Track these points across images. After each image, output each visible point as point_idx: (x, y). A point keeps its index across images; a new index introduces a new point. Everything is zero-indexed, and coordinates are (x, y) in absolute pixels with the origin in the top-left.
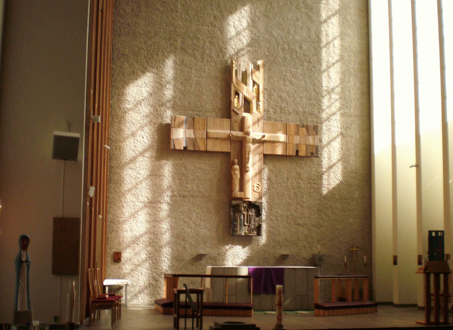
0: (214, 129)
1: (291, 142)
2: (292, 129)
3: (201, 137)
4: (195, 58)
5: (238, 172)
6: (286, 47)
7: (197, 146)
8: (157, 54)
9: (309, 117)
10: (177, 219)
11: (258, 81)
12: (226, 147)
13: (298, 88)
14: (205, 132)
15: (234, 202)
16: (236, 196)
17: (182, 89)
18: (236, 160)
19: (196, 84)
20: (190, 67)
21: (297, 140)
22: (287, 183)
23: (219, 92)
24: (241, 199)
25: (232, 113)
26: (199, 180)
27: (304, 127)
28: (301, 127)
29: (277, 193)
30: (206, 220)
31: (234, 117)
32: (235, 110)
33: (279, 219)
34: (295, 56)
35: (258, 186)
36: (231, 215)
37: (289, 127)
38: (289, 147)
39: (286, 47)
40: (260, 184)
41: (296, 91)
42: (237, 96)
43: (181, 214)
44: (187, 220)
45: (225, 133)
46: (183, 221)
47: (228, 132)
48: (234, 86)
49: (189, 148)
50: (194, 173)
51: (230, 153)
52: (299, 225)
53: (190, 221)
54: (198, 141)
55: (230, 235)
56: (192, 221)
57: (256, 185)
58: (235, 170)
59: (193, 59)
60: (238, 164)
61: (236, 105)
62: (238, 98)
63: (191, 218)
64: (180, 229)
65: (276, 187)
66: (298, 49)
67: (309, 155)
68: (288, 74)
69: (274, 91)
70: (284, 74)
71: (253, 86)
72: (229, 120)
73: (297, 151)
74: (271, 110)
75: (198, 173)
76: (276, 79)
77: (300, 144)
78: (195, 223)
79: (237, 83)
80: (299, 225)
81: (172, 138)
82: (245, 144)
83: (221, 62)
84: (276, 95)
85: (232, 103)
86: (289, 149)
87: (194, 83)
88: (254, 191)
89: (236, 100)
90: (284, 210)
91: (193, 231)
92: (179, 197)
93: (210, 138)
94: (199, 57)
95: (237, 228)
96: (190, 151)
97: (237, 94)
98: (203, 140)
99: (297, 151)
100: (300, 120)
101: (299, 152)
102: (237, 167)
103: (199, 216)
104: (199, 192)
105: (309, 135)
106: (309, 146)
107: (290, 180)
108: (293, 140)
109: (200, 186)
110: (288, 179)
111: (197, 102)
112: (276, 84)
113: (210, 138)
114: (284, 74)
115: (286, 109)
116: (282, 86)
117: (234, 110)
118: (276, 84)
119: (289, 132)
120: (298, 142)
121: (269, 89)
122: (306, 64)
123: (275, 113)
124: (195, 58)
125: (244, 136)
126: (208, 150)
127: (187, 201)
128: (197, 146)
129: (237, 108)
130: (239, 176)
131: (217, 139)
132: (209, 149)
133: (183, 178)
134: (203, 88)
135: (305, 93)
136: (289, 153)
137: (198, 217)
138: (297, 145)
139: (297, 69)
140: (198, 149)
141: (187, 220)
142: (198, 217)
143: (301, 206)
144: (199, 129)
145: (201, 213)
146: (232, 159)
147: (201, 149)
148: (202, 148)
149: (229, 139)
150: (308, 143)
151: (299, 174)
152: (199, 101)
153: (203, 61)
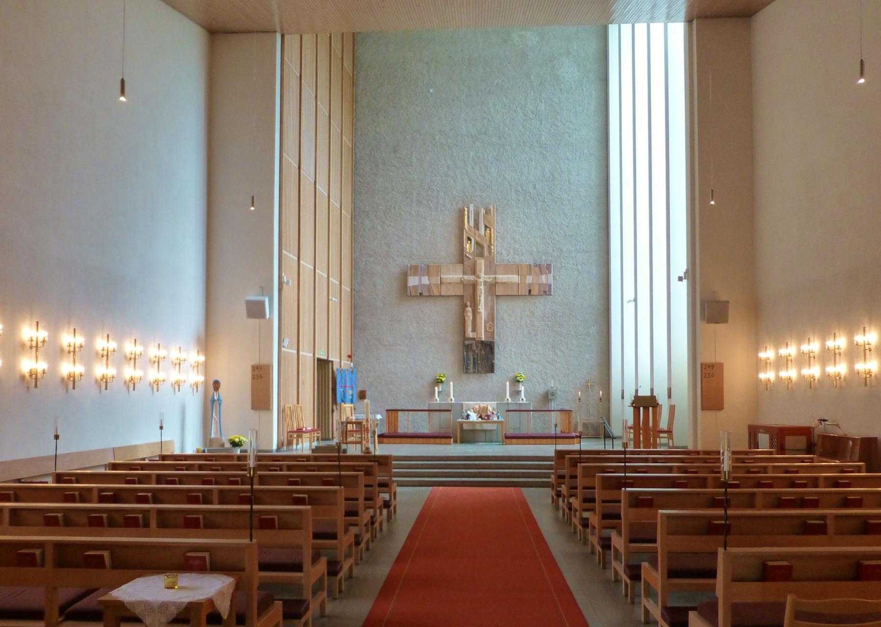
4: (430, 208)
5: (470, 314)
6: (520, 189)
8: (394, 208)
12: (459, 291)
15: (467, 342)
18: (469, 304)
21: (529, 279)
23: (453, 238)
24: (473, 339)
31: (466, 263)
34: (528, 197)
39: (520, 189)
49: (424, 294)
52: (532, 361)
57: (488, 325)
66: (531, 190)
68: (522, 216)
73: (530, 291)
74: (504, 252)
80: (532, 361)
89: (468, 245)
97: (469, 239)
99: (530, 291)
102: (469, 309)
122: (540, 204)
124: (430, 208)
130: (471, 318)
138: (530, 284)
148: (436, 293)
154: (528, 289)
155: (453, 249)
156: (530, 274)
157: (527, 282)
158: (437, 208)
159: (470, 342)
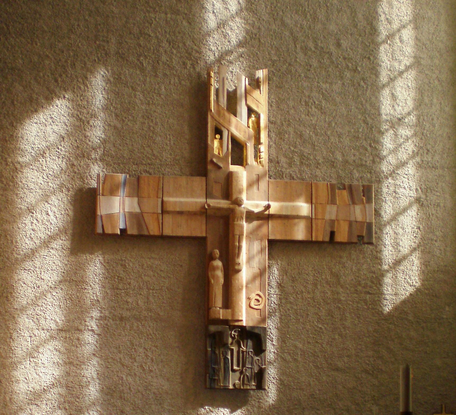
0: (177, 196)
1: (320, 217)
2: (323, 193)
3: (151, 211)
4: (142, 70)
5: (220, 274)
7: (145, 228)
9: (355, 171)
10: (110, 360)
11: (258, 107)
12: (197, 229)
13: (334, 118)
14: (160, 200)
15: (213, 328)
16: (217, 316)
17: (119, 126)
19: (143, 117)
20: (132, 88)
21: (331, 212)
22: (314, 293)
23: (186, 129)
24: (225, 322)
25: (210, 167)
26: (149, 289)
27: (344, 189)
28: (339, 189)
29: (296, 310)
30: (162, 361)
31: (213, 175)
32: (215, 160)
33: (299, 359)
35: (258, 298)
36: (207, 351)
37: (317, 190)
38: (317, 225)
40: (261, 294)
41: (330, 123)
42: (218, 136)
43: (115, 351)
44: (127, 361)
45: (196, 202)
46: (121, 363)
47: (203, 200)
48: (212, 117)
50: (140, 276)
51: (204, 239)
53: (132, 363)
54: (146, 219)
55: (206, 388)
56: (136, 364)
58: (215, 269)
59: (138, 72)
60: (221, 258)
61: (216, 152)
62: (221, 138)
63: (135, 359)
64: (116, 378)
65: (292, 299)
67: (355, 240)
68: (315, 94)
69: (289, 125)
70: (307, 94)
71: (249, 116)
72: (204, 178)
73: (332, 234)
75: (148, 276)
76: (291, 104)
77: (338, 220)
78: (141, 366)
79: (219, 112)
81: (99, 213)
82: (234, 221)
83: (190, 75)
84: (292, 133)
85: (209, 149)
86: (317, 230)
87: (140, 115)
88: (250, 307)
89: (216, 143)
90: (309, 343)
91: (138, 382)
92: (113, 320)
93: (168, 212)
94: (149, 68)
95: (218, 376)
96: (132, 236)
98: (155, 216)
99: (332, 234)
100: (339, 177)
101: (336, 234)
102: (218, 263)
103: (150, 354)
104: (150, 310)
105: (354, 203)
106: (354, 224)
107: (319, 287)
108: (324, 213)
109: (151, 299)
110: (315, 285)
111: (146, 149)
112: (292, 111)
113: (168, 212)
114: (307, 94)
115: (312, 158)
116: (303, 116)
117: (212, 161)
118: (292, 111)
119: (316, 198)
120: (333, 217)
121: (279, 121)
122: (348, 74)
123: (290, 165)
124: (142, 70)
125: (231, 206)
126: (164, 234)
127: (128, 327)
128: (145, 228)
129: (218, 157)
130: (222, 281)
131: (181, 213)
132: (168, 232)
133: (120, 286)
134: (156, 124)
135: (347, 128)
136: (316, 236)
137: (147, 356)
139: (331, 84)
140: (146, 233)
141: (127, 361)
142: (147, 356)
143: (341, 335)
144: (149, 197)
145: (154, 348)
146: (209, 249)
147: (152, 233)
148: (154, 230)
149: (203, 213)
150: (352, 219)
151: (336, 276)
152: (149, 146)
153: (156, 76)
154: (329, 229)
155: (185, 150)
156: (333, 202)
157: (327, 217)
158: (155, 69)
159: (219, 328)
